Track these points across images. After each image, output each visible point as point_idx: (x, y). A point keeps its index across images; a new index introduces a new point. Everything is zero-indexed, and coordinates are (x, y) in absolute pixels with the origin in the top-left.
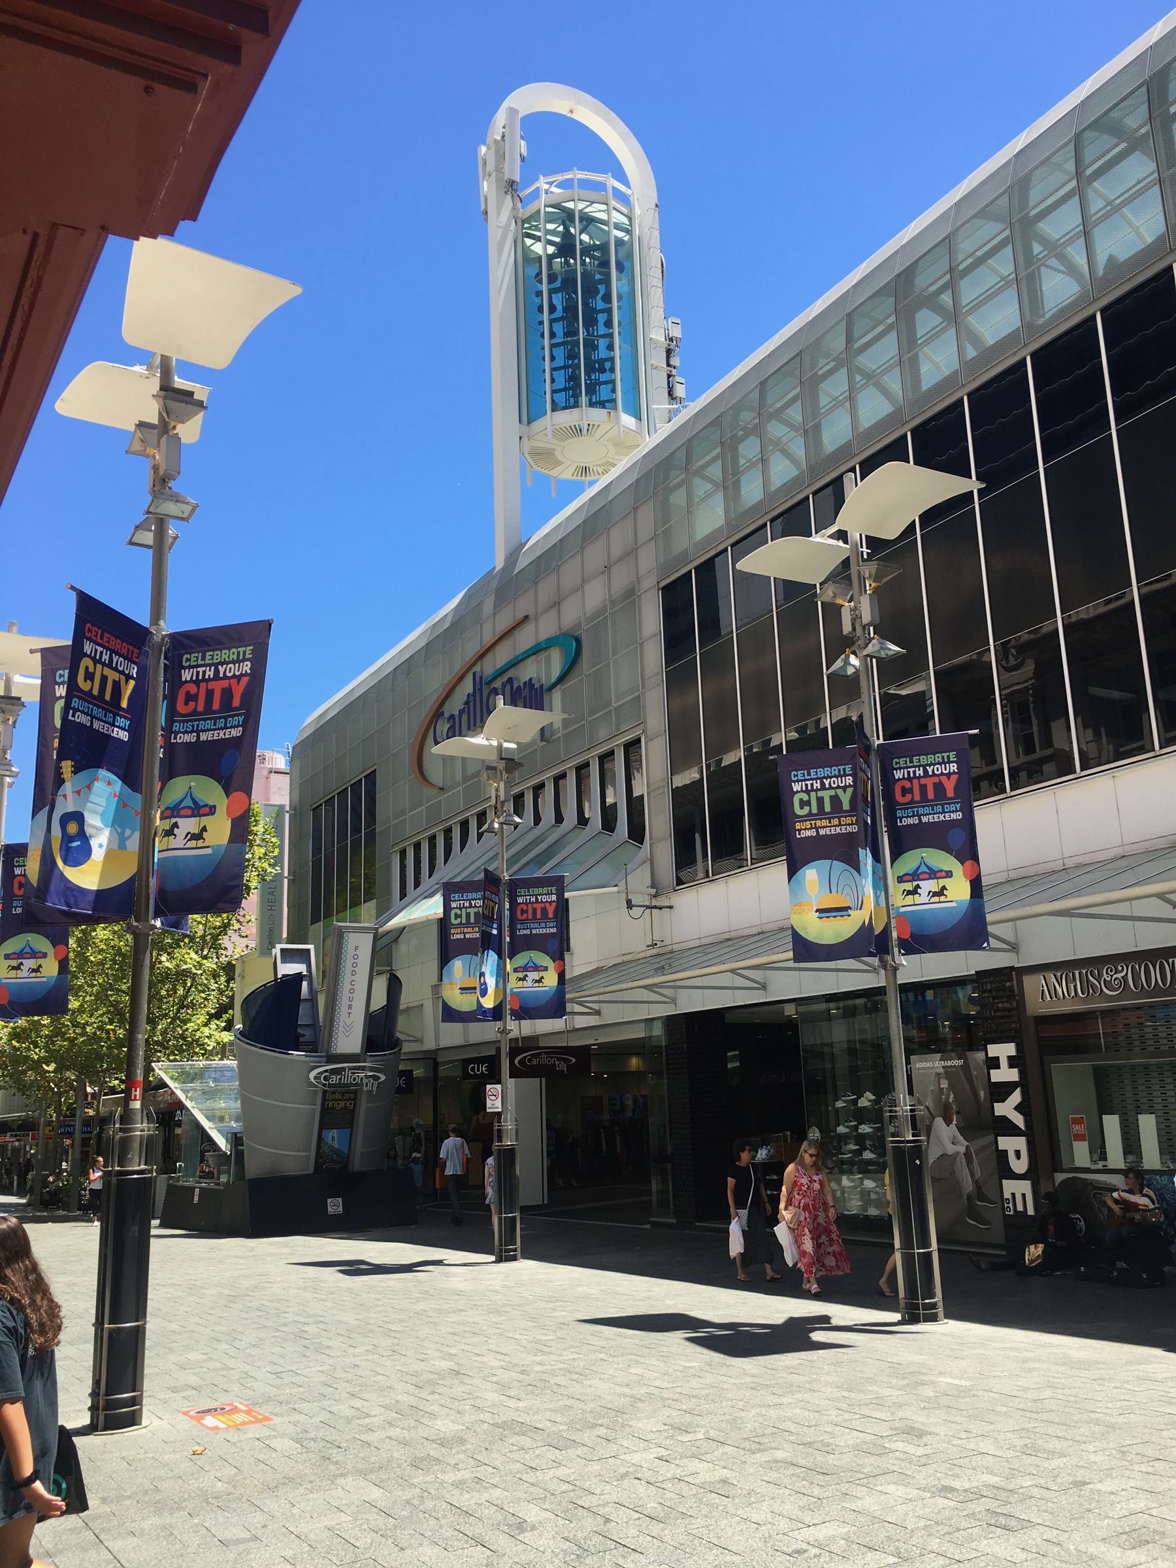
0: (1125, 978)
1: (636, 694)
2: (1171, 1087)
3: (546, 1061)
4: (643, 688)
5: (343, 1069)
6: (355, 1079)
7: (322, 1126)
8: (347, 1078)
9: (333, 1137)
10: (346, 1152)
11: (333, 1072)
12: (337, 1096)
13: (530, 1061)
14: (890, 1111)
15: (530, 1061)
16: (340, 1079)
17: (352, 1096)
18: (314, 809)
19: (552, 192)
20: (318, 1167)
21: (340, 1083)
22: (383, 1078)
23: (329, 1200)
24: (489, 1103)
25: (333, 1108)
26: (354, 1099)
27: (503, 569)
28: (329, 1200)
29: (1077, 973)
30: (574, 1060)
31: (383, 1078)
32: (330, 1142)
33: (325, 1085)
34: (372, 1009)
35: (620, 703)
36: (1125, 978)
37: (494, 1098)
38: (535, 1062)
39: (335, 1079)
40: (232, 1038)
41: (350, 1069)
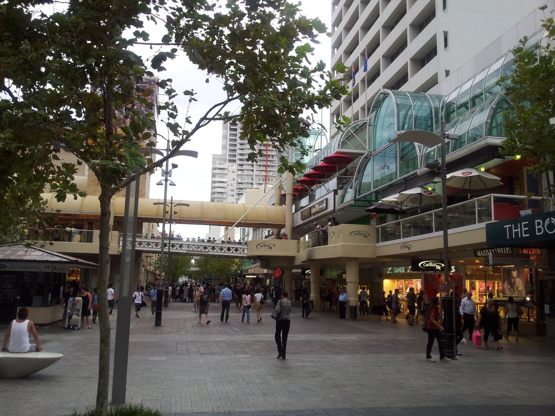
15: (425, 265)
28: (549, 313)
30: (443, 265)
38: (427, 265)
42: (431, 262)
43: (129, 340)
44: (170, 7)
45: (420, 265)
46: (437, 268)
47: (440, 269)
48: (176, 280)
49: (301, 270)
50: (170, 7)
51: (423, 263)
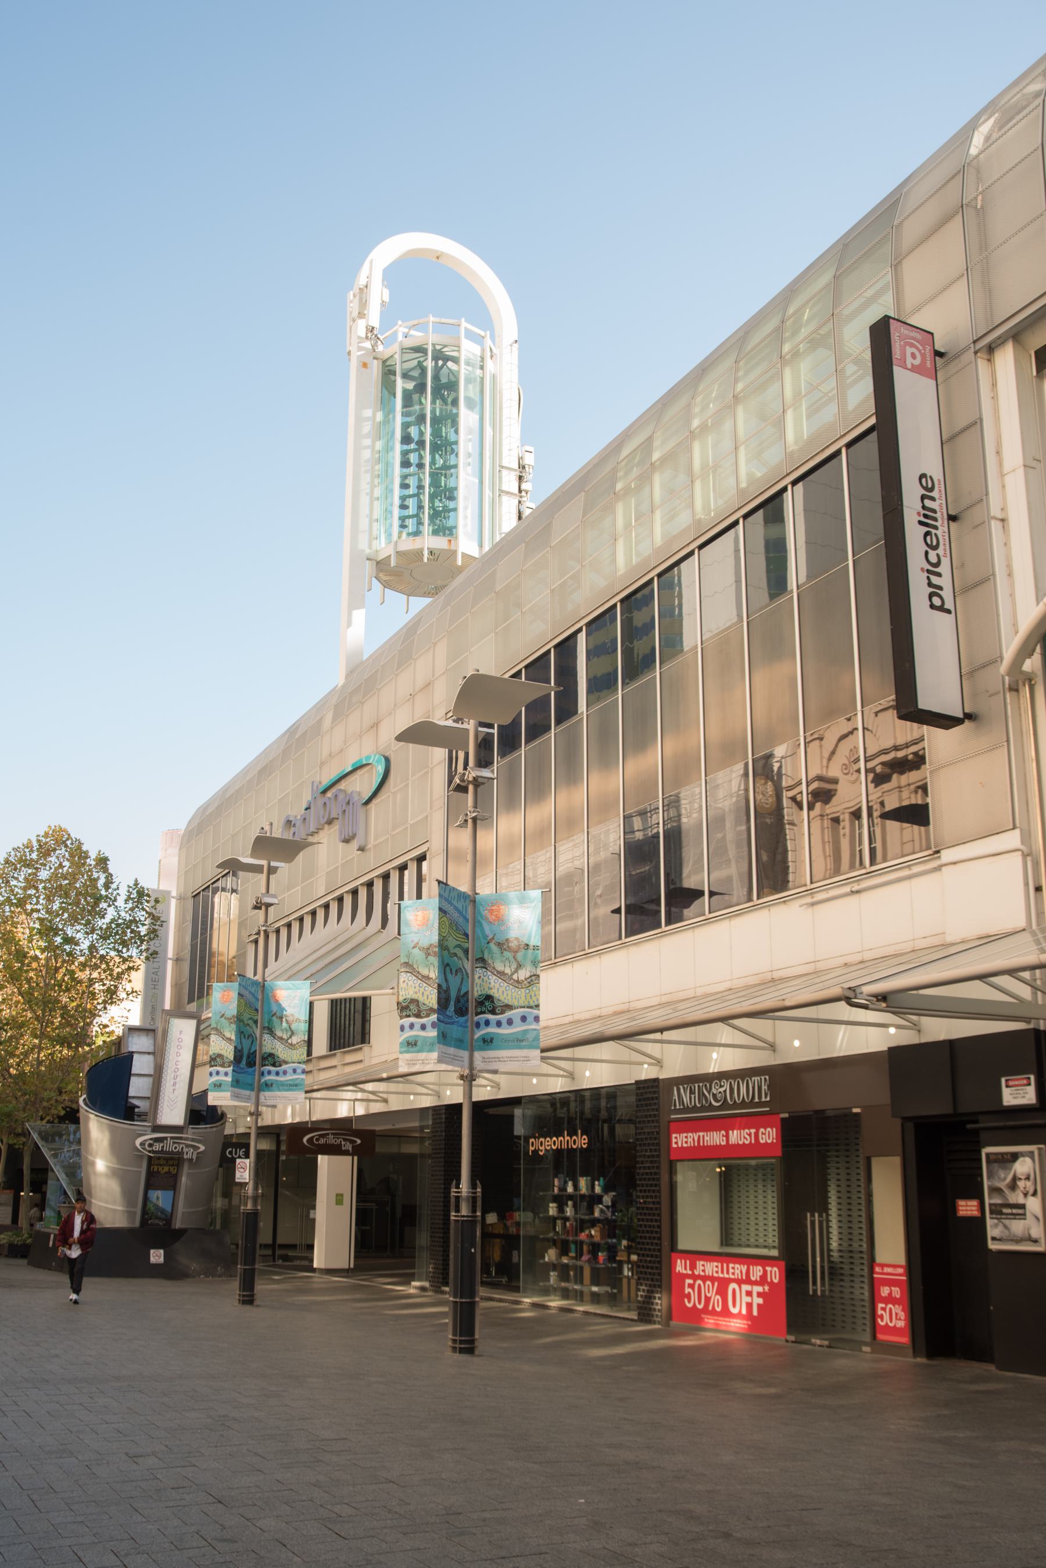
0: (725, 1091)
1: (424, 815)
2: (583, 1182)
3: (333, 1142)
4: (431, 808)
5: (166, 1138)
6: (176, 1148)
7: (148, 1186)
8: (170, 1146)
9: (160, 1198)
10: (170, 1211)
11: (157, 1140)
12: (162, 1162)
13: (317, 1140)
14: (456, 1192)
15: (317, 1140)
16: (163, 1147)
17: (175, 1162)
18: (194, 896)
19: (412, 336)
20: (144, 1221)
21: (162, 1150)
22: (202, 1148)
23: (152, 1251)
24: (238, 1175)
25: (158, 1172)
26: (178, 1165)
27: (343, 686)
28: (152, 1251)
29: (696, 1085)
30: (359, 1141)
31: (202, 1148)
32: (154, 1200)
33: (150, 1152)
34: (193, 1092)
35: (378, 842)
36: (725, 1091)
37: (242, 1170)
38: (322, 1141)
39: (157, 1147)
40: (528, 1036)
41: (172, 1138)
42: (332, 1134)
43: (411, 744)
44: (1038, 604)
45: (305, 1140)
46: (343, 1149)
47: (350, 1149)
48: (86, 1034)
49: (378, 1149)
50: (1038, 604)
51: (312, 1138)
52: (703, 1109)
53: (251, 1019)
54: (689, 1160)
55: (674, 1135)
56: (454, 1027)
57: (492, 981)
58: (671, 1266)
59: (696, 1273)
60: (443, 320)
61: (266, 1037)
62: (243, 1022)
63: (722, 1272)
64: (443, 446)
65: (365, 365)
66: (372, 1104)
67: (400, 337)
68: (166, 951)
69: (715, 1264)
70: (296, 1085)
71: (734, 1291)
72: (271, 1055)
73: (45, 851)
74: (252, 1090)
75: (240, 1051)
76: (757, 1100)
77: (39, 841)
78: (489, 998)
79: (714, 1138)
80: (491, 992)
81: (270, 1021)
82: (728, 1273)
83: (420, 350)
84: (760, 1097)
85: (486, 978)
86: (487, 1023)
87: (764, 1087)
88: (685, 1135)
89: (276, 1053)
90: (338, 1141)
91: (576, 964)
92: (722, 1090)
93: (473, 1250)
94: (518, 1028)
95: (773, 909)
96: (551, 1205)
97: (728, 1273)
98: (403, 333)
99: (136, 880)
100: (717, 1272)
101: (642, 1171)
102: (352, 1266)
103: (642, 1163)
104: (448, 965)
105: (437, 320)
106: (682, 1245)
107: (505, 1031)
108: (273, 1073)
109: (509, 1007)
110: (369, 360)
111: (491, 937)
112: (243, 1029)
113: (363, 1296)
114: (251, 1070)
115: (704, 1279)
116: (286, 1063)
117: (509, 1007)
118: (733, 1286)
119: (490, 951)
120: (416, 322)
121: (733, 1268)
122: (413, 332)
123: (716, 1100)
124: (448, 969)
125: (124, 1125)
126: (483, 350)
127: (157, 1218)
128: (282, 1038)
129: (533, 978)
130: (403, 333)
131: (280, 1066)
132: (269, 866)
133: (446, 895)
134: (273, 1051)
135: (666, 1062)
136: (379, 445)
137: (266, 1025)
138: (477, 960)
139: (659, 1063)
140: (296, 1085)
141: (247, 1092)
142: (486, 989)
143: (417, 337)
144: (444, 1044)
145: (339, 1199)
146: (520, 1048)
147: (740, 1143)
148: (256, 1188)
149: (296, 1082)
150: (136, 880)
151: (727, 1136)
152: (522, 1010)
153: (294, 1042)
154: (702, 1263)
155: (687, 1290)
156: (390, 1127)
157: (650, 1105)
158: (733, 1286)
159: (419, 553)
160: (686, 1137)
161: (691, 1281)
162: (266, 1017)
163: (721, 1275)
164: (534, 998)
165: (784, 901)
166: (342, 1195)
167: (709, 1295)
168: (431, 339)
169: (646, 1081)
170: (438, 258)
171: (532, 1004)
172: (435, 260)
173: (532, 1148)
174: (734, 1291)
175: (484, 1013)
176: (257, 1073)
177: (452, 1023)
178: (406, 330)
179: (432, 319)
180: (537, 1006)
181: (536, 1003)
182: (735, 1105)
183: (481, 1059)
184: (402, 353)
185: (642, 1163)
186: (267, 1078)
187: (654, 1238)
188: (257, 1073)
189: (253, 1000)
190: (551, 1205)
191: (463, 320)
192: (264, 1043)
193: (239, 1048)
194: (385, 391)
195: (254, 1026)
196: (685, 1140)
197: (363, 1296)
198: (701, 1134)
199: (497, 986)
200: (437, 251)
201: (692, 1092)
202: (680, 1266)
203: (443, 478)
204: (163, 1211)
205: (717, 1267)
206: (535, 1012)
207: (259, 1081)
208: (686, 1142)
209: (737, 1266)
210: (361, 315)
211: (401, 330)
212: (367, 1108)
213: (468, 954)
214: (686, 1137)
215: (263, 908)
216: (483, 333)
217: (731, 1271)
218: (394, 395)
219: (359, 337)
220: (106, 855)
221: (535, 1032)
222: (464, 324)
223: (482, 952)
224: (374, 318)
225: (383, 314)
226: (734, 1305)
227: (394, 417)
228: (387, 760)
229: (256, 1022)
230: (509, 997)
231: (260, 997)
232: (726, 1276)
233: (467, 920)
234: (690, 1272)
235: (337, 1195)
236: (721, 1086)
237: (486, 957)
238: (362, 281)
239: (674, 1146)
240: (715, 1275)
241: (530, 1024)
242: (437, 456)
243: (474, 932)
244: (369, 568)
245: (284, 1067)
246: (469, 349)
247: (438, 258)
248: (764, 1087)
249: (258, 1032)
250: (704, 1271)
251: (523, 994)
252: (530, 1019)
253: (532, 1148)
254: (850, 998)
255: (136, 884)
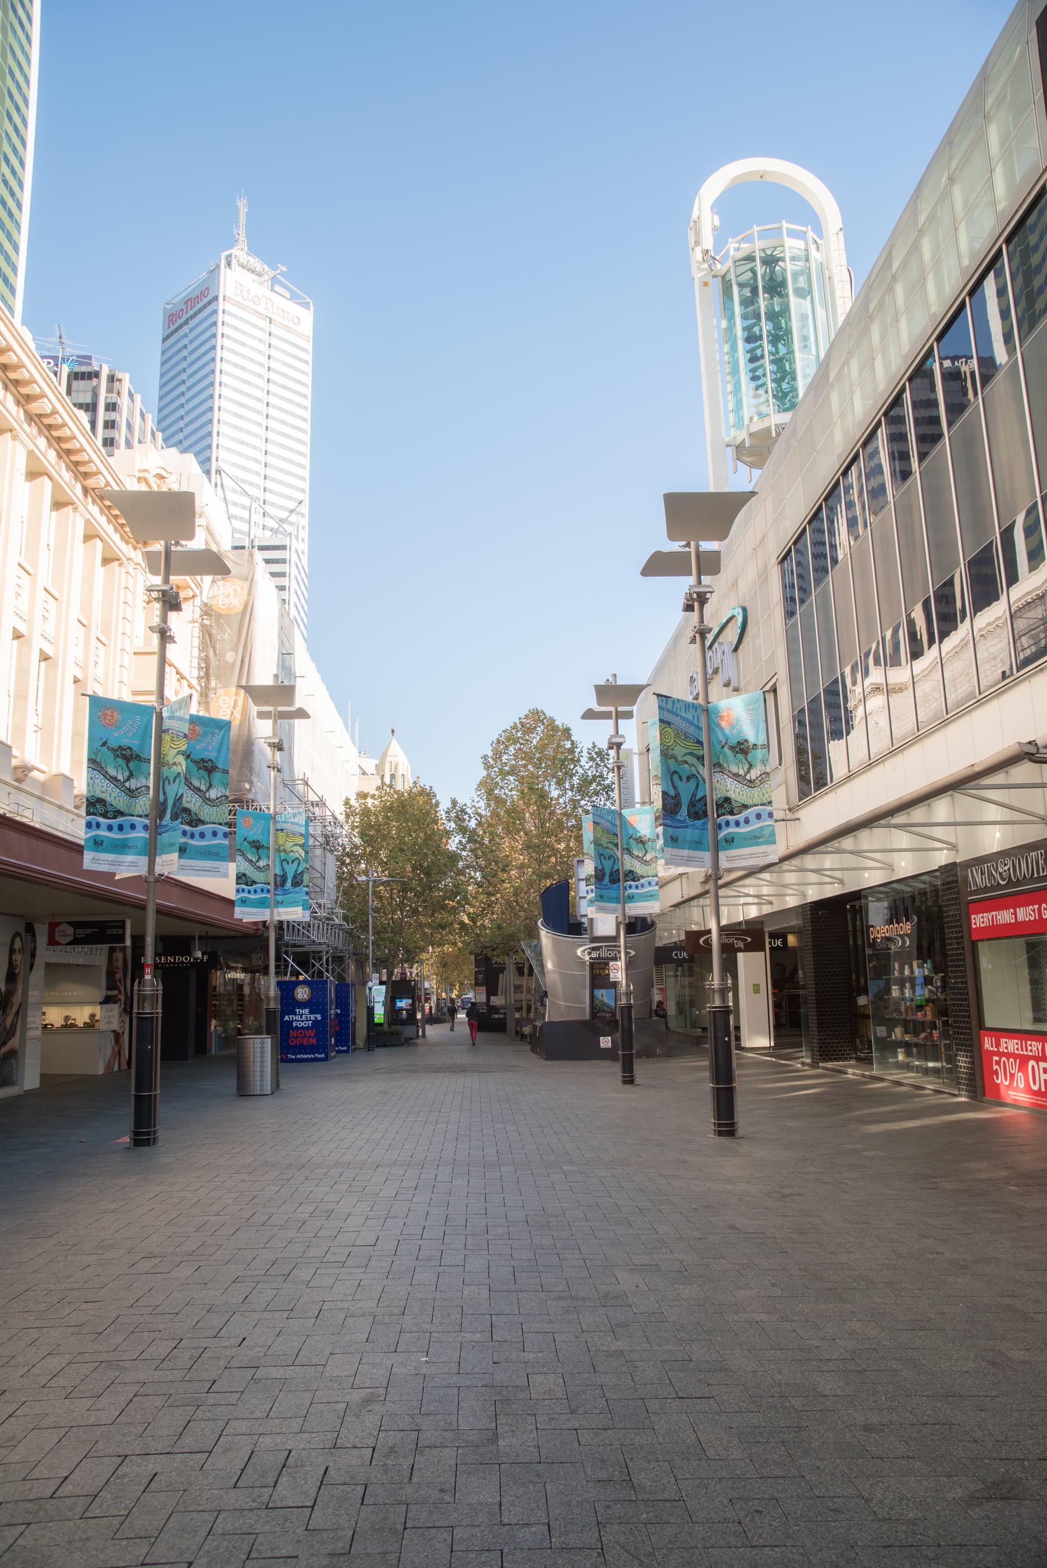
0: (1009, 869)
5: (601, 947)
23: (601, 1038)
25: (600, 975)
28: (601, 1038)
30: (749, 940)
36: (1009, 869)
37: (615, 971)
39: (594, 955)
41: (605, 946)
45: (701, 941)
52: (993, 888)
53: (610, 842)
54: (988, 940)
55: (973, 916)
56: (689, 830)
57: (728, 784)
58: (981, 1044)
59: (1001, 1050)
60: (766, 227)
61: (626, 857)
62: (602, 846)
63: (1022, 1050)
64: (780, 336)
65: (706, 284)
66: (764, 907)
67: (732, 253)
68: (633, 796)
69: (1016, 1041)
70: (652, 896)
71: (1033, 1067)
72: (631, 872)
73: (529, 730)
74: (619, 903)
75: (601, 870)
76: (1036, 875)
77: (521, 722)
78: (727, 800)
79: (1005, 917)
80: (728, 795)
81: (628, 843)
82: (1027, 1051)
83: (750, 258)
84: (1038, 873)
85: (723, 782)
86: (727, 824)
87: (1041, 862)
88: (981, 915)
89: (635, 870)
90: (731, 941)
91: (887, 763)
92: (1006, 868)
93: (726, 1039)
94: (755, 826)
95: (1033, 680)
96: (893, 987)
97: (1027, 1051)
98: (735, 248)
99: (594, 743)
100: (1018, 1049)
101: (951, 952)
102: (772, 1044)
103: (951, 944)
104: (675, 772)
105: (761, 228)
106: (989, 1023)
107: (743, 829)
108: (634, 887)
109: (746, 807)
110: (710, 279)
111: (724, 742)
112: (602, 851)
113: (766, 1071)
114: (614, 886)
115: (1009, 1055)
116: (643, 877)
117: (746, 807)
118: (1032, 1063)
119: (725, 756)
120: (744, 235)
121: (1031, 1045)
122: (743, 245)
123: (1003, 880)
124: (676, 777)
125: (567, 939)
126: (807, 244)
127: (604, 1011)
128: (638, 857)
129: (763, 776)
130: (735, 248)
131: (639, 880)
132: (617, 712)
133: (669, 706)
134: (632, 869)
135: (960, 847)
136: (726, 348)
137: (625, 846)
138: (714, 765)
139: (953, 847)
140: (652, 896)
141: (613, 905)
142: (724, 792)
143: (746, 248)
144: (674, 847)
145: (756, 989)
146: (758, 844)
147: (1027, 919)
148: (628, 986)
149: (652, 893)
150: (594, 743)
151: (1015, 914)
152: (756, 808)
153: (648, 859)
154: (1005, 1040)
155: (995, 1067)
156: (786, 925)
157: (952, 888)
158: (1032, 1063)
159: (768, 430)
160: (982, 917)
161: (997, 1058)
162: (625, 840)
163: (1021, 1053)
164: (766, 796)
165: (1041, 670)
166: (758, 985)
167: (1013, 1072)
168: (758, 246)
169: (946, 866)
170: (761, 177)
171: (765, 801)
172: (760, 179)
173: (872, 937)
174: (1033, 1067)
175: (724, 814)
176: (621, 888)
177: (686, 827)
178: (737, 245)
179: (756, 228)
180: (770, 803)
181: (769, 800)
182: (1019, 883)
183: (725, 859)
184: (735, 266)
185: (951, 944)
186: (629, 891)
187: (965, 1016)
188: (621, 888)
189: (610, 826)
190: (893, 987)
191: (784, 221)
192: (625, 862)
193: (600, 867)
194: (726, 298)
195: (615, 848)
196: (982, 920)
197: (766, 1071)
198: (994, 913)
199: (733, 787)
200: (759, 171)
201: (983, 873)
202: (988, 1044)
203: (787, 364)
204: (608, 1006)
205: (1017, 1044)
206: (769, 808)
207: (624, 894)
208: (983, 922)
209: (1034, 1043)
210: (697, 243)
211: (732, 245)
212: (760, 910)
213: (703, 760)
214: (982, 917)
215: (615, 747)
216: (804, 229)
217: (1029, 1048)
218: (733, 301)
219: (698, 262)
220: (569, 726)
221: (771, 828)
222: (785, 225)
223: (718, 757)
224: (708, 243)
225: (715, 238)
226: (1035, 1083)
227: (734, 322)
228: (744, 609)
229: (616, 845)
230: (745, 797)
231: (618, 823)
232: (1026, 1053)
233: (700, 729)
234: (996, 1049)
235: (754, 985)
236: (1005, 865)
237: (721, 761)
238: (695, 215)
239: (974, 926)
240: (1016, 1052)
241: (765, 821)
242: (780, 346)
243: (709, 739)
244: (730, 452)
245: (642, 881)
246: (792, 246)
247: (761, 177)
248: (1041, 862)
249: (619, 854)
250: (1006, 1048)
251: (756, 793)
252: (765, 816)
253: (872, 937)
254: (1033, 754)
255: (594, 747)
